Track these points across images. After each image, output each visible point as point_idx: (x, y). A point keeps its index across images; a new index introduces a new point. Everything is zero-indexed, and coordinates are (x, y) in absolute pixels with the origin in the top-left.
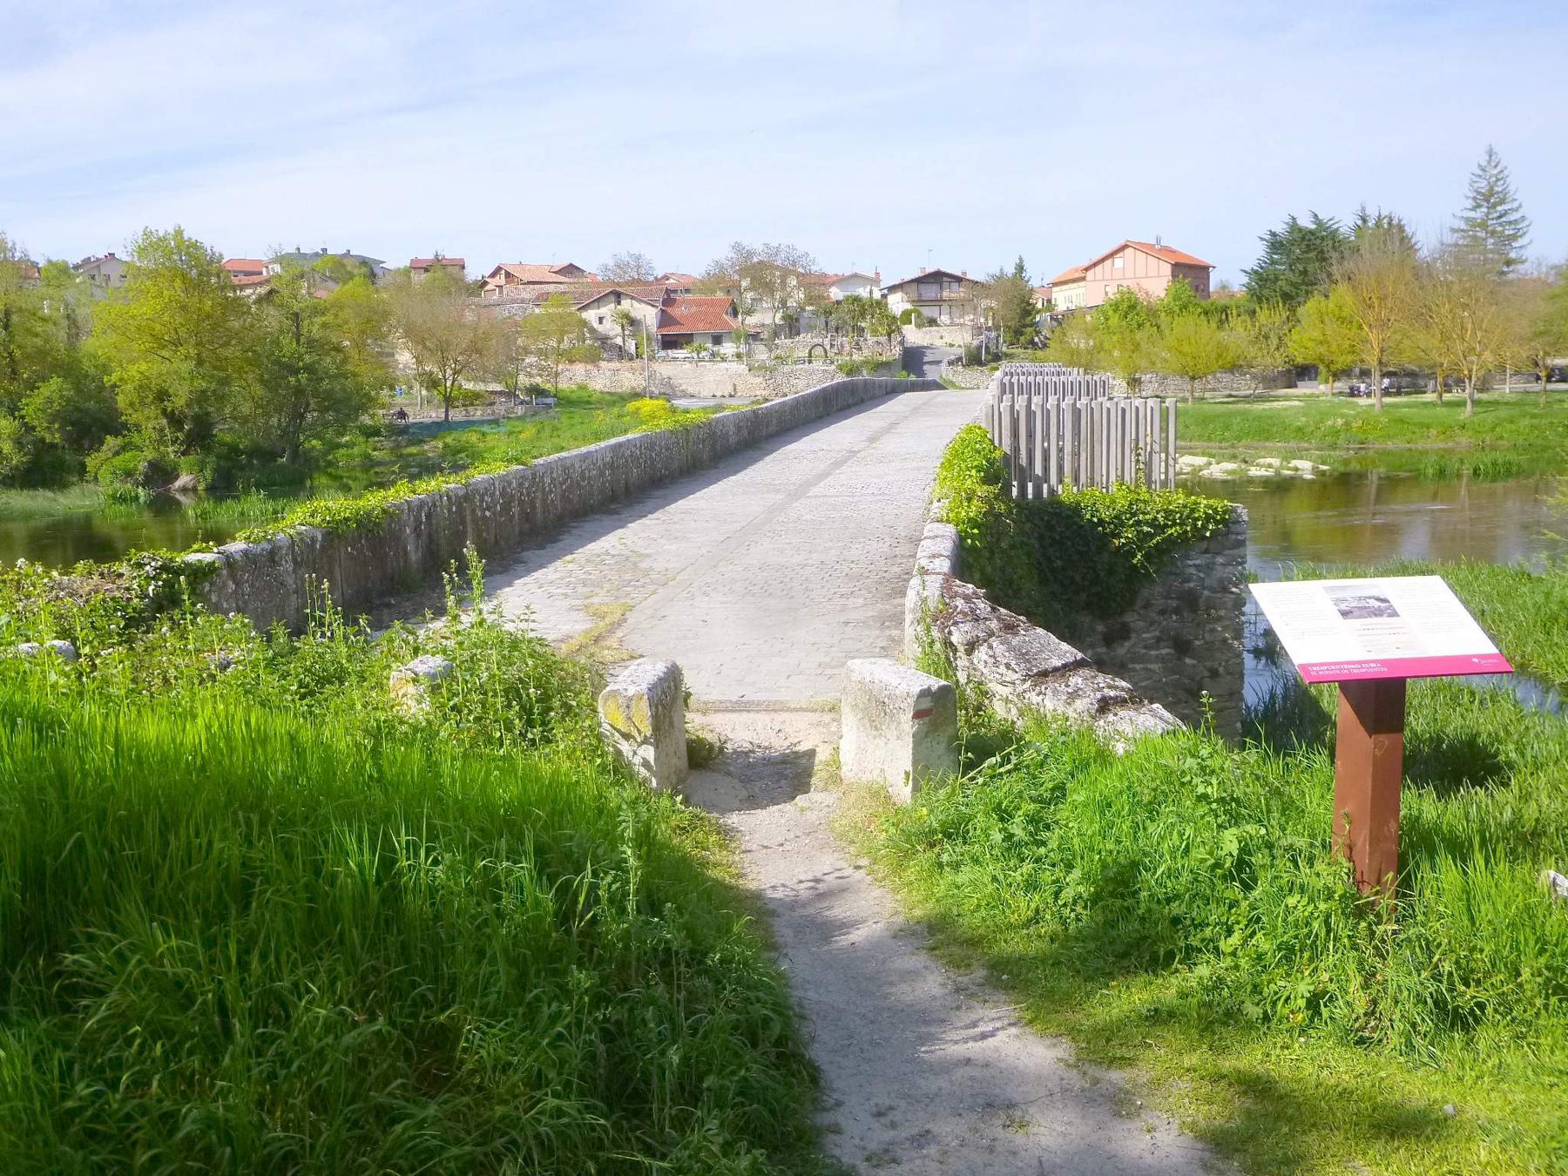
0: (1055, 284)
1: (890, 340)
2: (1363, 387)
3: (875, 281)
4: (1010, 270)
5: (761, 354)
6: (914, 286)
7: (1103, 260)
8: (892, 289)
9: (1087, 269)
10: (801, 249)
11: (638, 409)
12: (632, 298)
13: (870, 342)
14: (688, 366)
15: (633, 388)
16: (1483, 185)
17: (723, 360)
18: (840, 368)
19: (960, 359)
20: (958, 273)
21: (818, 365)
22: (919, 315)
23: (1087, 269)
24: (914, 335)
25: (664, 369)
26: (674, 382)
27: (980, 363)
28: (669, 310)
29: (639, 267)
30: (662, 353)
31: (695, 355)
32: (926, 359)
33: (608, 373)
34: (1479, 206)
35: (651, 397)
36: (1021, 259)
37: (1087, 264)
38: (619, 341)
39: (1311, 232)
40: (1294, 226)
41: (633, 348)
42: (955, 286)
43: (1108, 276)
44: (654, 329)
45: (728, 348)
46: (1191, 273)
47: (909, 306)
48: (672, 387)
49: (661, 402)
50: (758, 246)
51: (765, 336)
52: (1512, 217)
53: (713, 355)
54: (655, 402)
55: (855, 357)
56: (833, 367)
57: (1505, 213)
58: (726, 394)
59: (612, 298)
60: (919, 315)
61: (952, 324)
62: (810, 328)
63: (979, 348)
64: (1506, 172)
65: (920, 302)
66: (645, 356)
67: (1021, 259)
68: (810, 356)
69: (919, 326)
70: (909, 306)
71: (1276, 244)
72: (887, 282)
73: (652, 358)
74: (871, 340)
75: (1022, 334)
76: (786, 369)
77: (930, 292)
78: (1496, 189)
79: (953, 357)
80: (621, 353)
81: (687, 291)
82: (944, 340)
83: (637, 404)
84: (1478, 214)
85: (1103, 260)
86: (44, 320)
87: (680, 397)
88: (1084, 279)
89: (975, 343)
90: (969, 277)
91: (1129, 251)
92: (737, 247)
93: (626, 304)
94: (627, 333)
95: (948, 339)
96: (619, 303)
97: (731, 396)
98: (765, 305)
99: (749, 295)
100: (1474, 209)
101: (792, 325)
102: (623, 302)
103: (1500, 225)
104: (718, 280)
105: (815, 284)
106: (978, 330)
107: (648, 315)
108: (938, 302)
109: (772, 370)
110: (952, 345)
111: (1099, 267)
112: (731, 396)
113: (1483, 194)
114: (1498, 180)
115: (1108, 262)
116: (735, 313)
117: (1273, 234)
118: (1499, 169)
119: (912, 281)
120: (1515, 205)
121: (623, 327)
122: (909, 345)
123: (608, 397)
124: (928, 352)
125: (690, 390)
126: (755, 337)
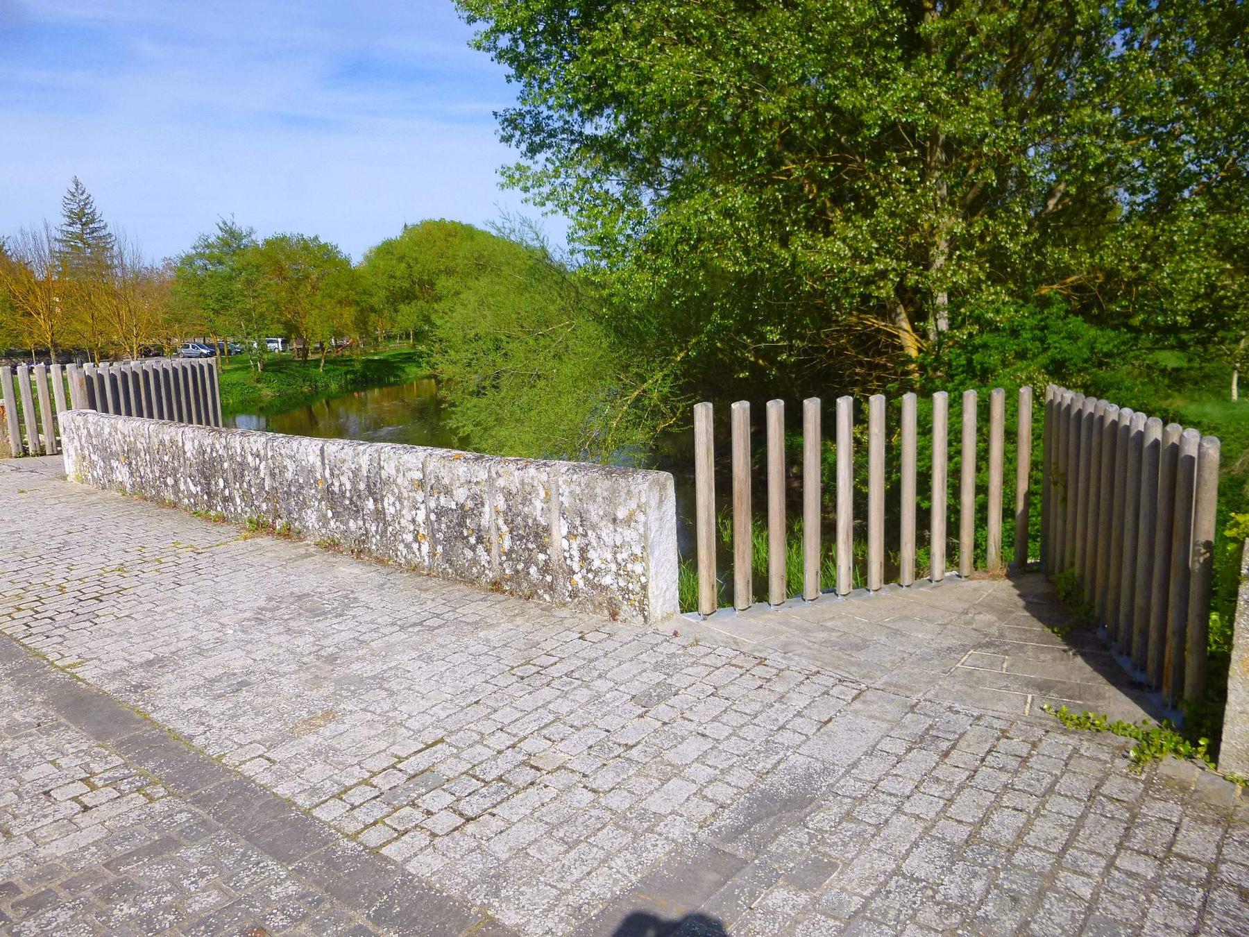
52: (103, 233)
64: (91, 199)
84: (77, 228)
114: (86, 204)
120: (102, 224)
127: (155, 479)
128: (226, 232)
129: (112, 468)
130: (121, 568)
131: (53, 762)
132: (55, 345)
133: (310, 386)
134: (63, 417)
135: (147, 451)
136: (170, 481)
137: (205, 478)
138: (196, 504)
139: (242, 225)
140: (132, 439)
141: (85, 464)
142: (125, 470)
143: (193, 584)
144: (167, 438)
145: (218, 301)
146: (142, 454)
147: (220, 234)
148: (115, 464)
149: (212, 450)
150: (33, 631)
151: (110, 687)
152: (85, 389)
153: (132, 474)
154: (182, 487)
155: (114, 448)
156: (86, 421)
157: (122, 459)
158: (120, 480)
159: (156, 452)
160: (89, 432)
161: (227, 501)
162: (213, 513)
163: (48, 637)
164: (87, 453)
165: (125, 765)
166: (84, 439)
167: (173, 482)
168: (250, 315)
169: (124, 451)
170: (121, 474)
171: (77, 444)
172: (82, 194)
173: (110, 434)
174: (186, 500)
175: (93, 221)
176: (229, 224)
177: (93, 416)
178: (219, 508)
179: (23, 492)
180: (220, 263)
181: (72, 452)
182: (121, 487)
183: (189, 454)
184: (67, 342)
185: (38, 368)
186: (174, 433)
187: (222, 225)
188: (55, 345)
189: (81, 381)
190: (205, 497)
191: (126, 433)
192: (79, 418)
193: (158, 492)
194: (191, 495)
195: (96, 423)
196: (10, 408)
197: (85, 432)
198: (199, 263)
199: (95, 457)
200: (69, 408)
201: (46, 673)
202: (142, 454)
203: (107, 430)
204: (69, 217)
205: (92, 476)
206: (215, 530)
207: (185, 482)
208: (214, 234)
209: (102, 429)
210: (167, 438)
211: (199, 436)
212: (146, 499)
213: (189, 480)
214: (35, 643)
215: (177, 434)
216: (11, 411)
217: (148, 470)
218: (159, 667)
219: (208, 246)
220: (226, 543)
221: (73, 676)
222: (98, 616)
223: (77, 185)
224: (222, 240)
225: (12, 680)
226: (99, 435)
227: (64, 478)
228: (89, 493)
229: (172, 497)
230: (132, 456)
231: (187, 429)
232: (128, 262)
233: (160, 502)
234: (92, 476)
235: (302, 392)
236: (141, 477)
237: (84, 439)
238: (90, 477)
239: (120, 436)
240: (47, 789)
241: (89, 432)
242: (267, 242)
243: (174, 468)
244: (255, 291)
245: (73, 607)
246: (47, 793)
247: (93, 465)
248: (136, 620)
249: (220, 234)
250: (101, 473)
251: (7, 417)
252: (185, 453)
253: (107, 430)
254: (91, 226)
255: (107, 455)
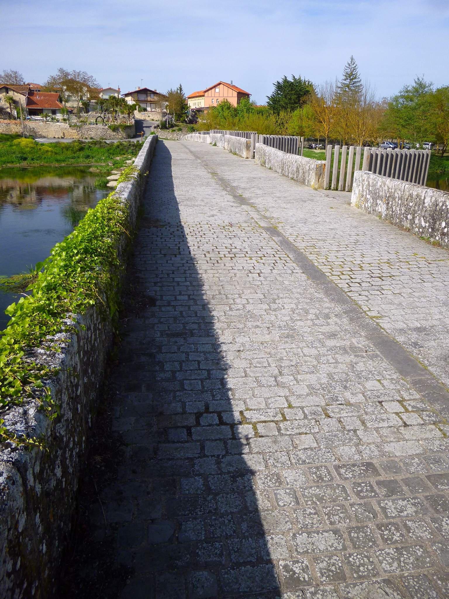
0: (189, 98)
1: (129, 116)
2: (314, 145)
3: (118, 92)
4: (170, 90)
5: (74, 120)
6: (136, 95)
7: (211, 89)
8: (127, 95)
9: (205, 92)
10: (90, 74)
11: (20, 143)
12: (14, 91)
13: (121, 117)
14: (41, 123)
15: (17, 132)
16: (349, 71)
17: (58, 121)
18: (110, 127)
19: (158, 126)
20: (153, 90)
21: (100, 126)
22: (140, 107)
23: (205, 92)
24: (138, 115)
25: (31, 124)
26: (36, 130)
27: (167, 128)
28: (31, 97)
29: (16, 77)
30: (29, 117)
31: (45, 119)
32: (144, 125)
33: (5, 125)
34: (347, 79)
35: (25, 137)
36: (180, 85)
37: (205, 89)
38: (9, 110)
39: (292, 83)
40: (285, 81)
41: (16, 114)
42: (152, 95)
43: (213, 95)
44: (25, 106)
45: (59, 116)
46: (242, 95)
47: (134, 103)
48: (35, 133)
49: (30, 140)
50: (70, 70)
51: (75, 111)
52: (358, 84)
53: (52, 119)
54: (28, 140)
55: (115, 123)
56: (107, 127)
57: (355, 82)
58: (60, 137)
59: (4, 90)
60: (140, 107)
61: (151, 111)
62: (94, 109)
63: (166, 121)
64: (357, 67)
65: (138, 101)
66: (21, 118)
67: (180, 85)
68: (96, 121)
69: (139, 111)
70: (134, 103)
71: (279, 87)
72: (124, 91)
73: (25, 119)
74: (121, 116)
75: (181, 117)
76: (86, 127)
77: (142, 97)
78: (353, 73)
79: (156, 125)
80: (10, 116)
81: (39, 91)
82: (150, 118)
83: (19, 140)
84: (347, 82)
85: (211, 89)
86: (400, 499)
87: (39, 138)
88: (203, 96)
89: (164, 119)
90: (158, 92)
91: (221, 86)
92: (61, 70)
93: (11, 93)
94: (12, 107)
95: (151, 117)
96: (8, 93)
97: (62, 138)
98: (74, 99)
99: (67, 93)
100: (345, 80)
101: (86, 107)
102: (9, 92)
103: (354, 87)
104: (49, 88)
105: (94, 92)
106: (164, 114)
107: (22, 99)
108: (146, 102)
109: (80, 127)
110: (153, 120)
111: (210, 92)
112: (62, 138)
113: (349, 74)
114: (354, 69)
115: (213, 90)
116: (61, 101)
117: (278, 83)
118: (355, 65)
119: (135, 92)
120: (359, 80)
121: (10, 104)
122: (136, 119)
123: (5, 136)
124: (144, 122)
125: (44, 134)
126: (71, 112)
127: (400, 214)
128: (418, 84)
129: (377, 204)
130: (388, 262)
131: (379, 381)
132: (328, 137)
133: (441, 170)
134: (357, 173)
135: (400, 198)
136: (410, 217)
137: (433, 219)
138: (422, 233)
139: (427, 81)
140: (393, 191)
141: (362, 199)
142: (384, 207)
143: (432, 282)
144: (415, 193)
145: (406, 121)
146: (397, 200)
147: (414, 85)
148: (379, 202)
149: (443, 205)
150: (352, 289)
151: (401, 339)
152: (369, 160)
153: (387, 209)
154: (417, 221)
155: (381, 193)
156: (369, 178)
157: (384, 200)
158: (380, 211)
159: (405, 200)
160: (369, 183)
161: (444, 235)
162: (432, 240)
163: (360, 295)
164: (365, 193)
165: (422, 401)
166: (365, 186)
167: (411, 218)
168: (421, 129)
169: (386, 196)
170: (382, 208)
171: (360, 188)
172: (353, 65)
173: (381, 186)
174: (417, 229)
175: (355, 78)
176: (421, 79)
177: (372, 176)
178: (437, 238)
179: (332, 208)
180: (411, 100)
181: (357, 192)
182: (380, 215)
183: (426, 205)
184: (333, 136)
185: (337, 147)
186: (420, 191)
187: (417, 80)
188: (328, 137)
189: (368, 156)
190: (430, 230)
191: (390, 187)
192: (365, 175)
193: (401, 222)
194: (420, 226)
195: (374, 180)
196: (328, 166)
197: (367, 183)
198: (401, 100)
199: (368, 197)
200: (360, 169)
201: (363, 317)
202: (397, 200)
203: (379, 184)
204: (345, 76)
205: (365, 206)
206: (435, 250)
207: (419, 219)
208: (411, 84)
209: (377, 183)
210: (415, 193)
211: (437, 196)
212: (392, 223)
213: (422, 218)
214: (355, 296)
215: (422, 192)
216: (328, 168)
217: (398, 209)
218: (425, 334)
219: (407, 92)
220: (443, 260)
221: (378, 324)
222: (383, 289)
223: (352, 60)
224: (414, 88)
225: (347, 316)
226: (374, 186)
227: (349, 204)
228: (362, 214)
229: (408, 225)
230: (391, 199)
231: (429, 190)
232: (368, 99)
233: (401, 227)
234: (365, 206)
235: (436, 173)
236: (393, 212)
237: (365, 186)
238: (363, 206)
239: (386, 188)
240: (380, 400)
241: (369, 183)
242: (438, 90)
243: (414, 211)
244: (426, 116)
245: (368, 280)
246: (380, 402)
247: (367, 200)
248: (404, 297)
249: (414, 85)
250: (370, 205)
251: (326, 170)
252: (424, 203)
253: (379, 184)
254: (354, 80)
255: (376, 196)
